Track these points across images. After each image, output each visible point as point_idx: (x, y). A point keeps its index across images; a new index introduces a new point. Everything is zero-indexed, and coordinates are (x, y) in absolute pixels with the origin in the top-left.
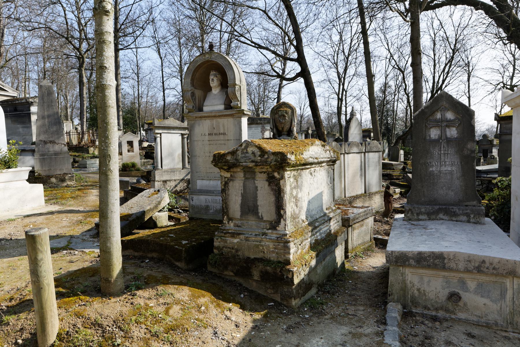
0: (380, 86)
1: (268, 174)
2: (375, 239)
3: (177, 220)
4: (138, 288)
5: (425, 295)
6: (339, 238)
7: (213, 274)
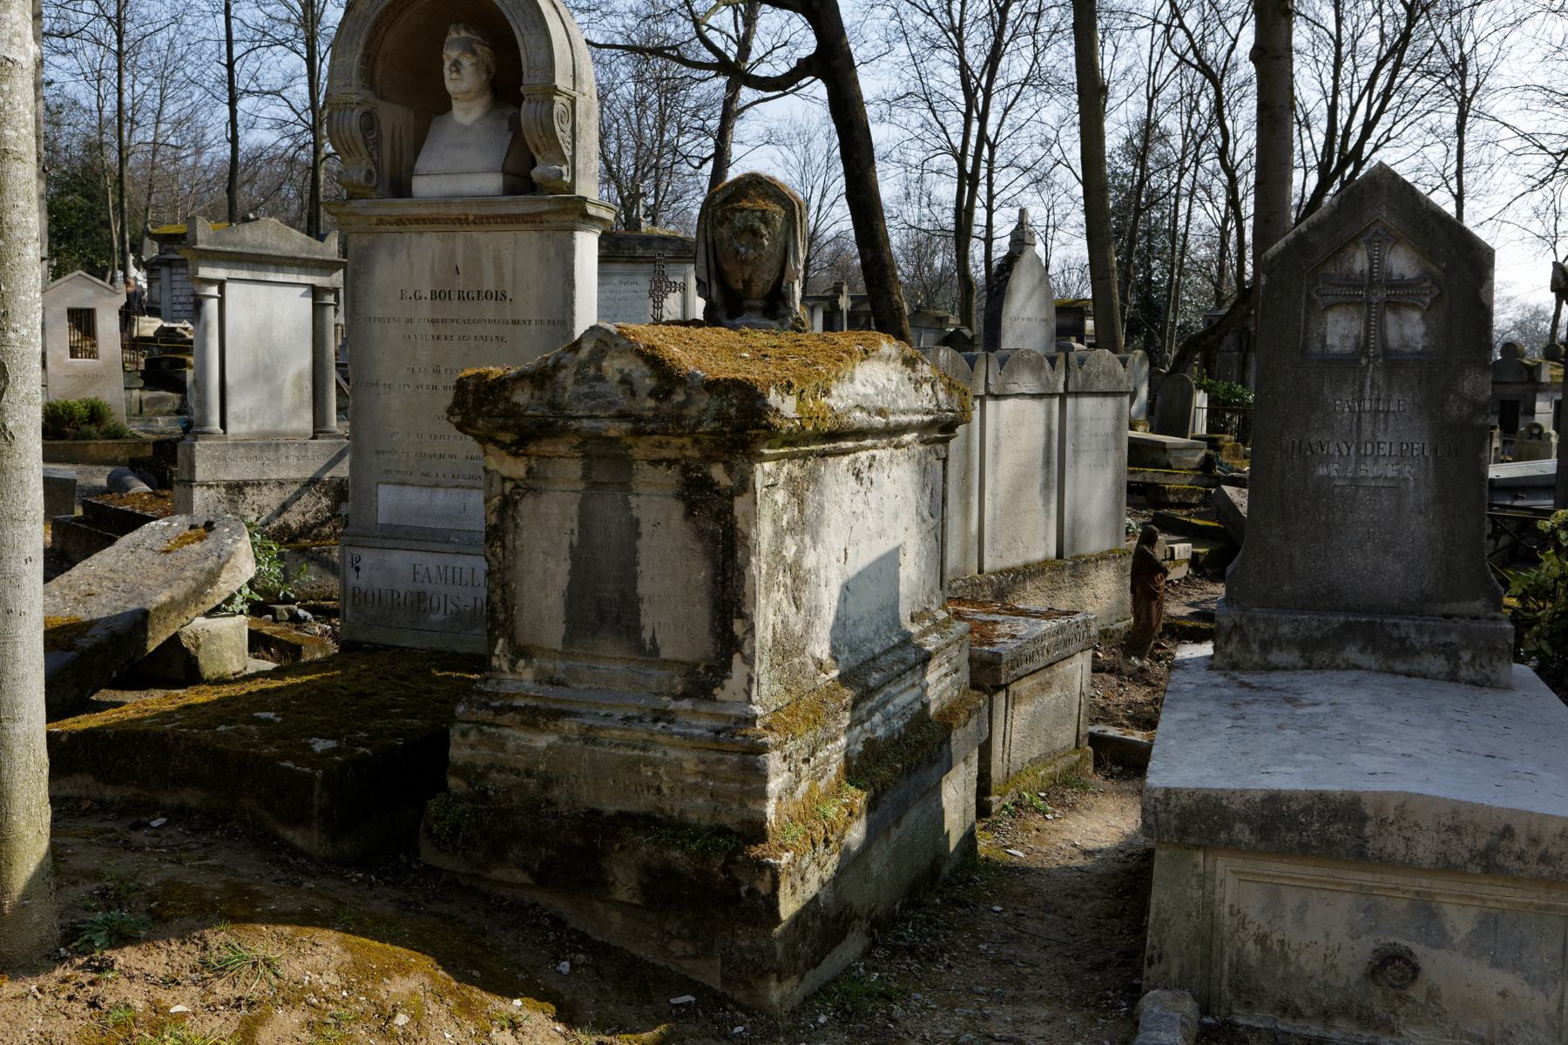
0: (1125, 131)
1: (685, 470)
2: (1096, 741)
3: (289, 653)
4: (121, 938)
5: (1285, 957)
6: (957, 736)
7: (444, 877)
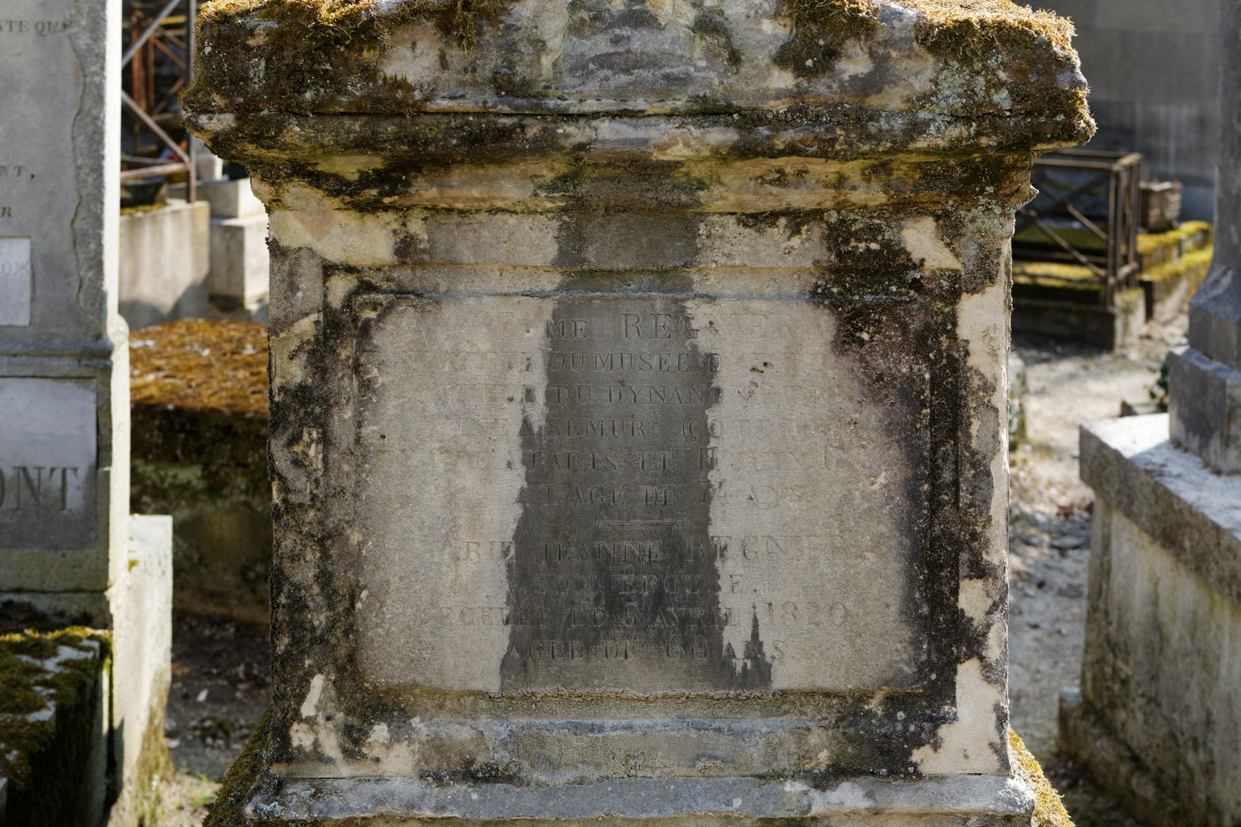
1: (837, 235)
